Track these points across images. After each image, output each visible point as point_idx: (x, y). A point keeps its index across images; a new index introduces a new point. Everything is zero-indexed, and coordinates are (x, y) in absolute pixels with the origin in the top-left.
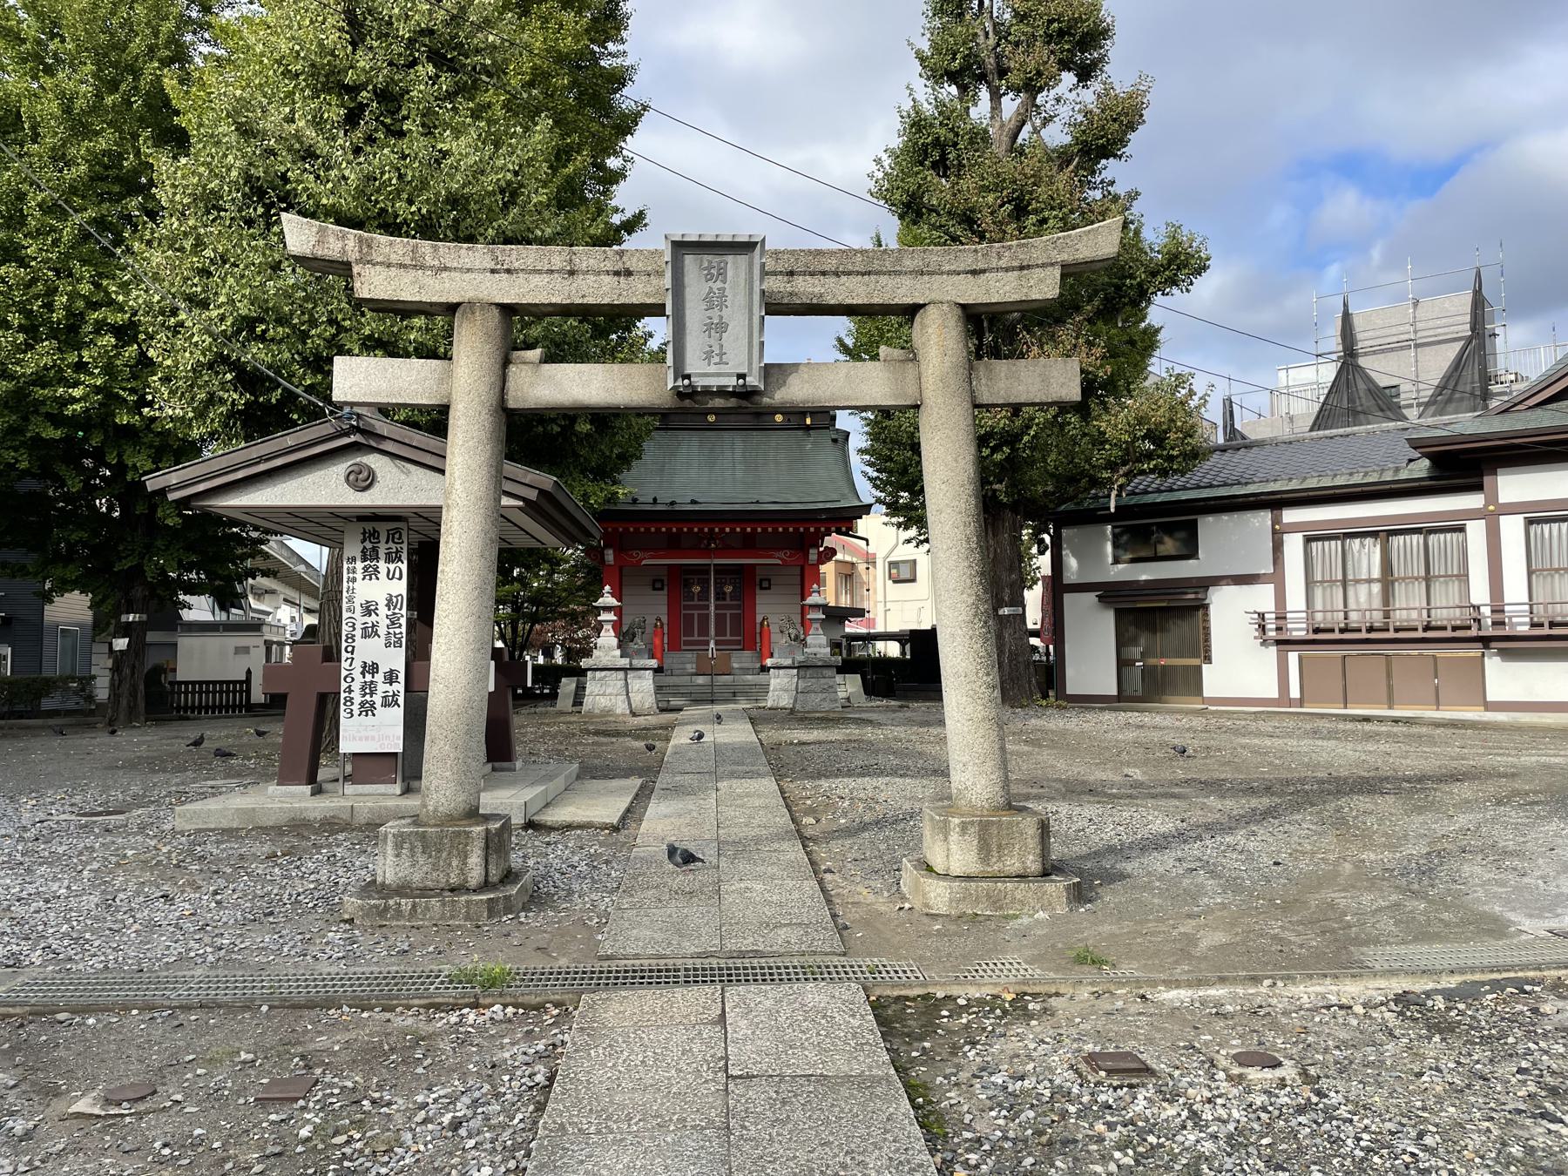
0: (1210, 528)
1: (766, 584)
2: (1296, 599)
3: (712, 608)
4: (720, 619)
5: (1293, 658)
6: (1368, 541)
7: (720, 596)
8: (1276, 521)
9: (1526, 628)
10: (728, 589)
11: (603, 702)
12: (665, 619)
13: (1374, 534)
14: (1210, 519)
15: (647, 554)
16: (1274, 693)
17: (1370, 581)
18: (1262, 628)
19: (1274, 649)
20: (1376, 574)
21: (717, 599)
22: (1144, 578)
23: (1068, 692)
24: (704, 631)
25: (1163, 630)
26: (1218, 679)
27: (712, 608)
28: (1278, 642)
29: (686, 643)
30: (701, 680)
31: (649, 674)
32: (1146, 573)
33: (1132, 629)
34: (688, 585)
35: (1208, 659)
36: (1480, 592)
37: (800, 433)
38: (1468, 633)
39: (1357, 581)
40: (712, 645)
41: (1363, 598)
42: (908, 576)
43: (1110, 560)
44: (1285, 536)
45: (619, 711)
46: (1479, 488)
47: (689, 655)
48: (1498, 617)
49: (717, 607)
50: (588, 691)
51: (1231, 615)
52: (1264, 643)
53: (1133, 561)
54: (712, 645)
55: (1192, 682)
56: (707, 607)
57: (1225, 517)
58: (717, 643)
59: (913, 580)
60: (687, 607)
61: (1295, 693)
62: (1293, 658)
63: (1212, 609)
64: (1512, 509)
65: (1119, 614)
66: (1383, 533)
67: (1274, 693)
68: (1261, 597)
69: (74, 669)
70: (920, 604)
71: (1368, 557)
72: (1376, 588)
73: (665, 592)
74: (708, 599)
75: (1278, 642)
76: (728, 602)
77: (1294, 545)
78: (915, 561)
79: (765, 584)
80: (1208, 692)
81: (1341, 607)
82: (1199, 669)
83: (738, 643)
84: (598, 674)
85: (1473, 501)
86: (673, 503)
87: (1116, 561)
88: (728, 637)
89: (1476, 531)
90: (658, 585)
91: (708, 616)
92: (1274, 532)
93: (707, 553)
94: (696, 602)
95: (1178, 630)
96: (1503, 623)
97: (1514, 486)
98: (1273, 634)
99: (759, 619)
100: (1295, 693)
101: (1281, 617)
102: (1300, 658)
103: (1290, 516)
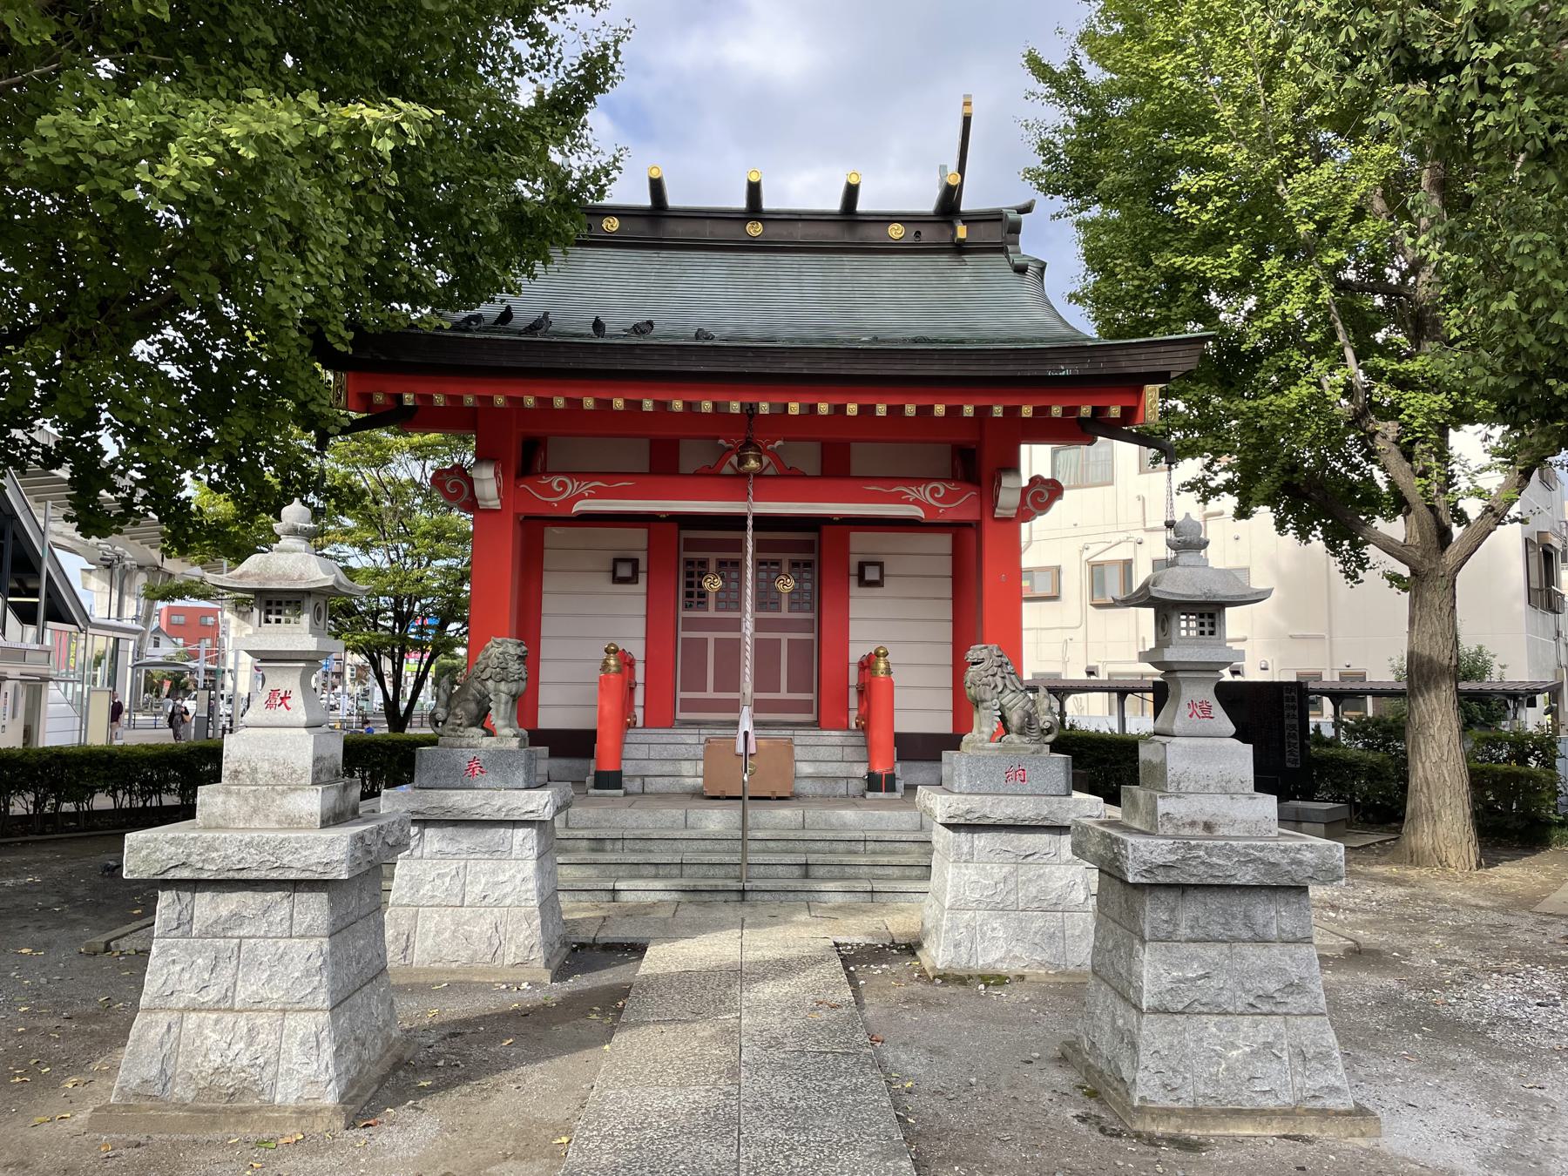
1: (871, 576)
3: (748, 626)
4: (766, 651)
7: (766, 599)
10: (786, 585)
11: (215, 1046)
12: (637, 650)
15: (586, 487)
21: (760, 605)
24: (729, 679)
27: (748, 626)
29: (689, 705)
30: (717, 820)
31: (523, 841)
34: (696, 570)
37: (944, 260)
40: (746, 724)
42: (1048, 592)
45: (287, 1093)
47: (691, 737)
49: (759, 625)
50: (153, 983)
54: (746, 724)
56: (737, 625)
58: (759, 706)
59: (1055, 598)
60: (691, 624)
70: (1068, 634)
73: (641, 586)
74: (738, 605)
76: (784, 614)
78: (1058, 570)
79: (872, 574)
83: (805, 707)
84: (206, 906)
86: (638, 329)
88: (783, 695)
90: (625, 571)
91: (737, 645)
93: (739, 483)
94: (711, 613)
99: (856, 653)
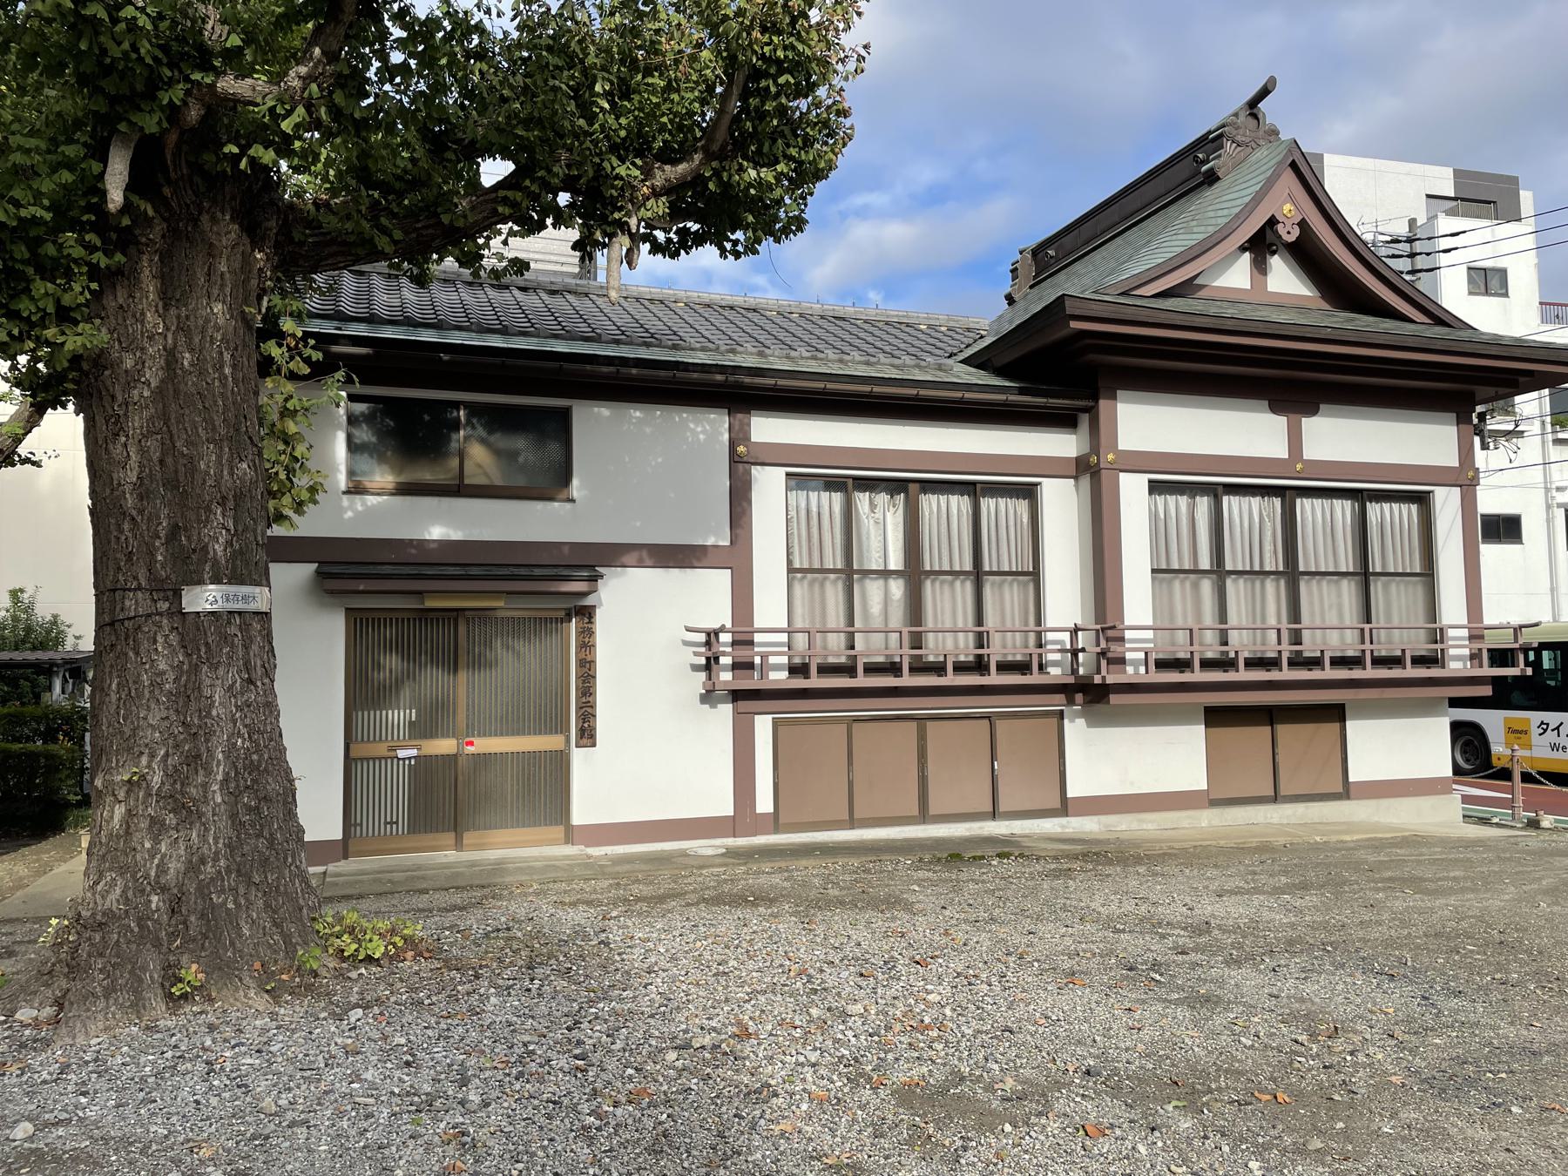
0: (598, 428)
2: (770, 609)
5: (763, 726)
6: (882, 498)
8: (738, 437)
9: (784, 674)
13: (896, 487)
14: (603, 411)
16: (726, 808)
17: (885, 574)
18: (710, 665)
19: (726, 709)
20: (896, 561)
22: (436, 533)
23: (338, 835)
25: (479, 663)
26: (603, 786)
28: (737, 696)
32: (441, 524)
33: (392, 663)
35: (587, 735)
36: (1065, 603)
38: (1034, 678)
39: (866, 573)
41: (876, 608)
43: (342, 480)
44: (756, 471)
46: (1065, 421)
48: (743, 653)
51: (645, 629)
52: (709, 697)
53: (404, 490)
55: (547, 789)
57: (636, 413)
61: (764, 803)
62: (763, 726)
63: (599, 615)
64: (1137, 462)
65: (360, 626)
66: (906, 484)
67: (726, 808)
68: (704, 597)
69: (955, 623)
71: (882, 527)
72: (897, 588)
75: (737, 696)
77: (769, 485)
80: (580, 815)
81: (842, 624)
82: (560, 763)
85: (1062, 444)
87: (356, 489)
89: (1061, 503)
92: (734, 459)
95: (515, 664)
96: (751, 666)
97: (1145, 424)
98: (726, 676)
100: (764, 803)
101: (743, 641)
102: (775, 723)
103: (768, 429)
